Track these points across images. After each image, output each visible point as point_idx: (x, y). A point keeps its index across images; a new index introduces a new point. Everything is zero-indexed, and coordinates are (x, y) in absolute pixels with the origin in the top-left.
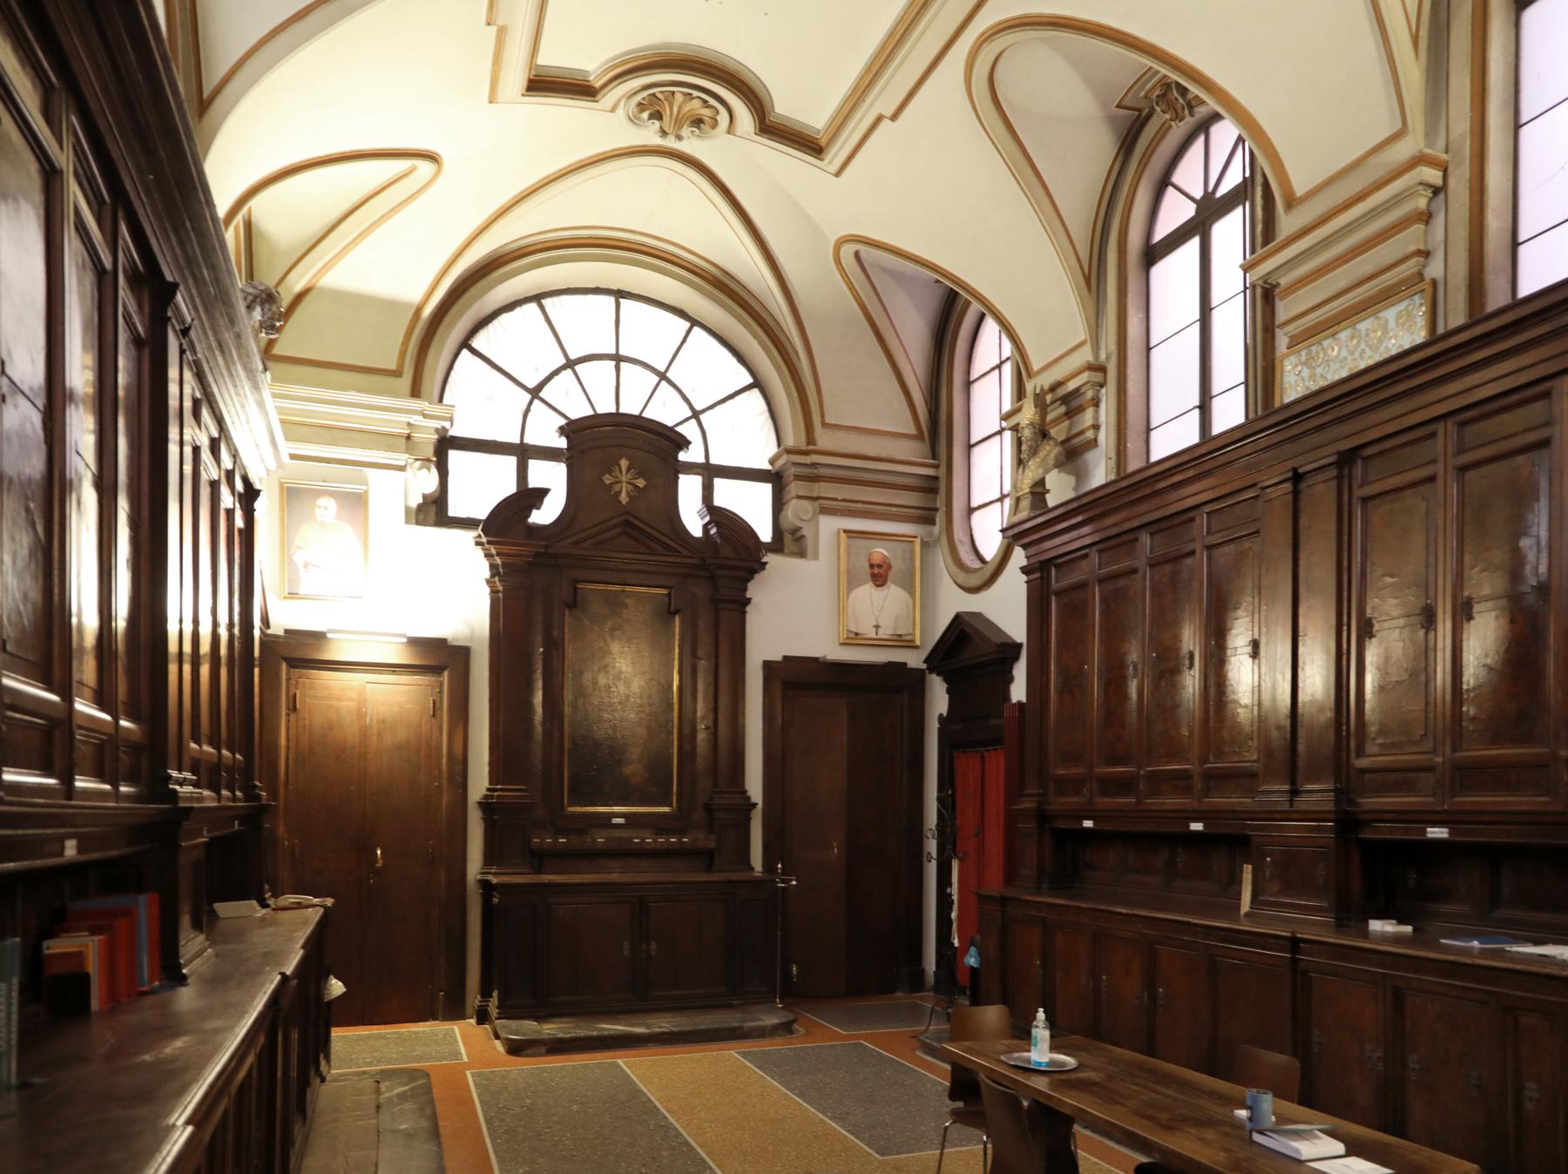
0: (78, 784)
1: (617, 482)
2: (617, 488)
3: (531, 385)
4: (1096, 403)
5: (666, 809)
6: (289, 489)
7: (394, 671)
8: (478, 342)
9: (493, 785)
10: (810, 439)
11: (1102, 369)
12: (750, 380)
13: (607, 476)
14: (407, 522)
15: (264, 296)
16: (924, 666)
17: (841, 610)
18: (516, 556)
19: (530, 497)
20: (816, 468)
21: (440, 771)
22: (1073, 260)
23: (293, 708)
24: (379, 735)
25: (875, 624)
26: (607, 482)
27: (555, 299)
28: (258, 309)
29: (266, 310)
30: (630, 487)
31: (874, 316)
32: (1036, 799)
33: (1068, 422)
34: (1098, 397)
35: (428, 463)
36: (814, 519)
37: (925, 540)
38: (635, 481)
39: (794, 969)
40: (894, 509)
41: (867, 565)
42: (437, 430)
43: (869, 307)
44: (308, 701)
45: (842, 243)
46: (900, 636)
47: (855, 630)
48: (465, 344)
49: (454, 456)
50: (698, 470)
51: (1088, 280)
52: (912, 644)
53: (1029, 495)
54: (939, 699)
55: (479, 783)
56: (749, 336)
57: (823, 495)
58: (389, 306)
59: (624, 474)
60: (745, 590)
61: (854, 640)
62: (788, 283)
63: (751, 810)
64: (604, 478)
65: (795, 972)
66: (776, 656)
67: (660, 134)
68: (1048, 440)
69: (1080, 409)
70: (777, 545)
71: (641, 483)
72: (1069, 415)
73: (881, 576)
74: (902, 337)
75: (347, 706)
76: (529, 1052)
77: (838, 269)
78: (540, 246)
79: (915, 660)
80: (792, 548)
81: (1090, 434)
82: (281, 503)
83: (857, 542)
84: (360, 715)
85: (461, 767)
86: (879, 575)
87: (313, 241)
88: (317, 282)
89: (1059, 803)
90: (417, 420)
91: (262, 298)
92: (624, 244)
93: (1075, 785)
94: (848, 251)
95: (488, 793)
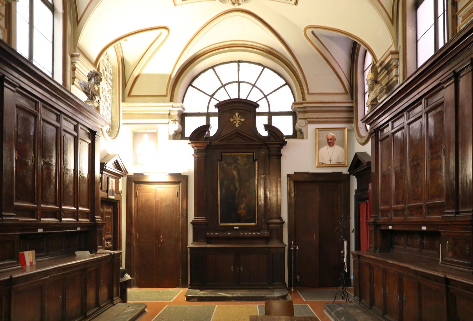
0: (80, 220)
1: (235, 121)
2: (235, 122)
3: (210, 94)
4: (397, 67)
5: (254, 224)
6: (135, 133)
7: (166, 184)
8: (194, 84)
9: (196, 217)
10: (304, 98)
11: (397, 53)
12: (285, 83)
13: (231, 119)
14: (169, 139)
15: (94, 74)
16: (348, 173)
17: (317, 156)
18: (201, 146)
19: (207, 127)
20: (306, 108)
21: (179, 213)
22: (384, 14)
23: (136, 196)
24: (161, 202)
25: (329, 159)
26: (231, 121)
27: (219, 67)
28: (93, 79)
29: (95, 78)
30: (239, 122)
31: (324, 53)
32: (374, 218)
33: (388, 76)
34: (398, 64)
35: (175, 121)
36: (306, 125)
37: (349, 128)
38: (241, 120)
39: (298, 277)
40: (336, 119)
41: (326, 139)
42: (178, 111)
43: (321, 50)
44: (140, 193)
45: (307, 29)
46: (340, 163)
47: (322, 162)
48: (190, 84)
49: (187, 119)
50: (266, 114)
51: (392, 21)
52: (344, 165)
53: (370, 105)
54: (354, 183)
55: (191, 216)
56: (283, 70)
57: (309, 117)
58: (162, 76)
59: (237, 118)
60: (281, 152)
61: (322, 165)
62: (290, 48)
63: (283, 224)
64: (230, 120)
65: (298, 278)
66: (292, 172)
67: (232, 4)
68: (378, 84)
69: (391, 70)
70: (295, 136)
71: (243, 120)
72: (388, 74)
73: (332, 143)
74: (336, 59)
75: (152, 195)
76: (192, 300)
77: (307, 39)
78: (210, 51)
79: (345, 171)
80: (300, 136)
81: (395, 79)
82: (133, 137)
83: (322, 132)
84: (156, 197)
85: (185, 212)
86: (331, 142)
87: (138, 62)
88: (141, 73)
89: (382, 219)
90: (171, 109)
91: (94, 75)
92: (237, 45)
93: (385, 212)
94: (309, 31)
95: (194, 219)
